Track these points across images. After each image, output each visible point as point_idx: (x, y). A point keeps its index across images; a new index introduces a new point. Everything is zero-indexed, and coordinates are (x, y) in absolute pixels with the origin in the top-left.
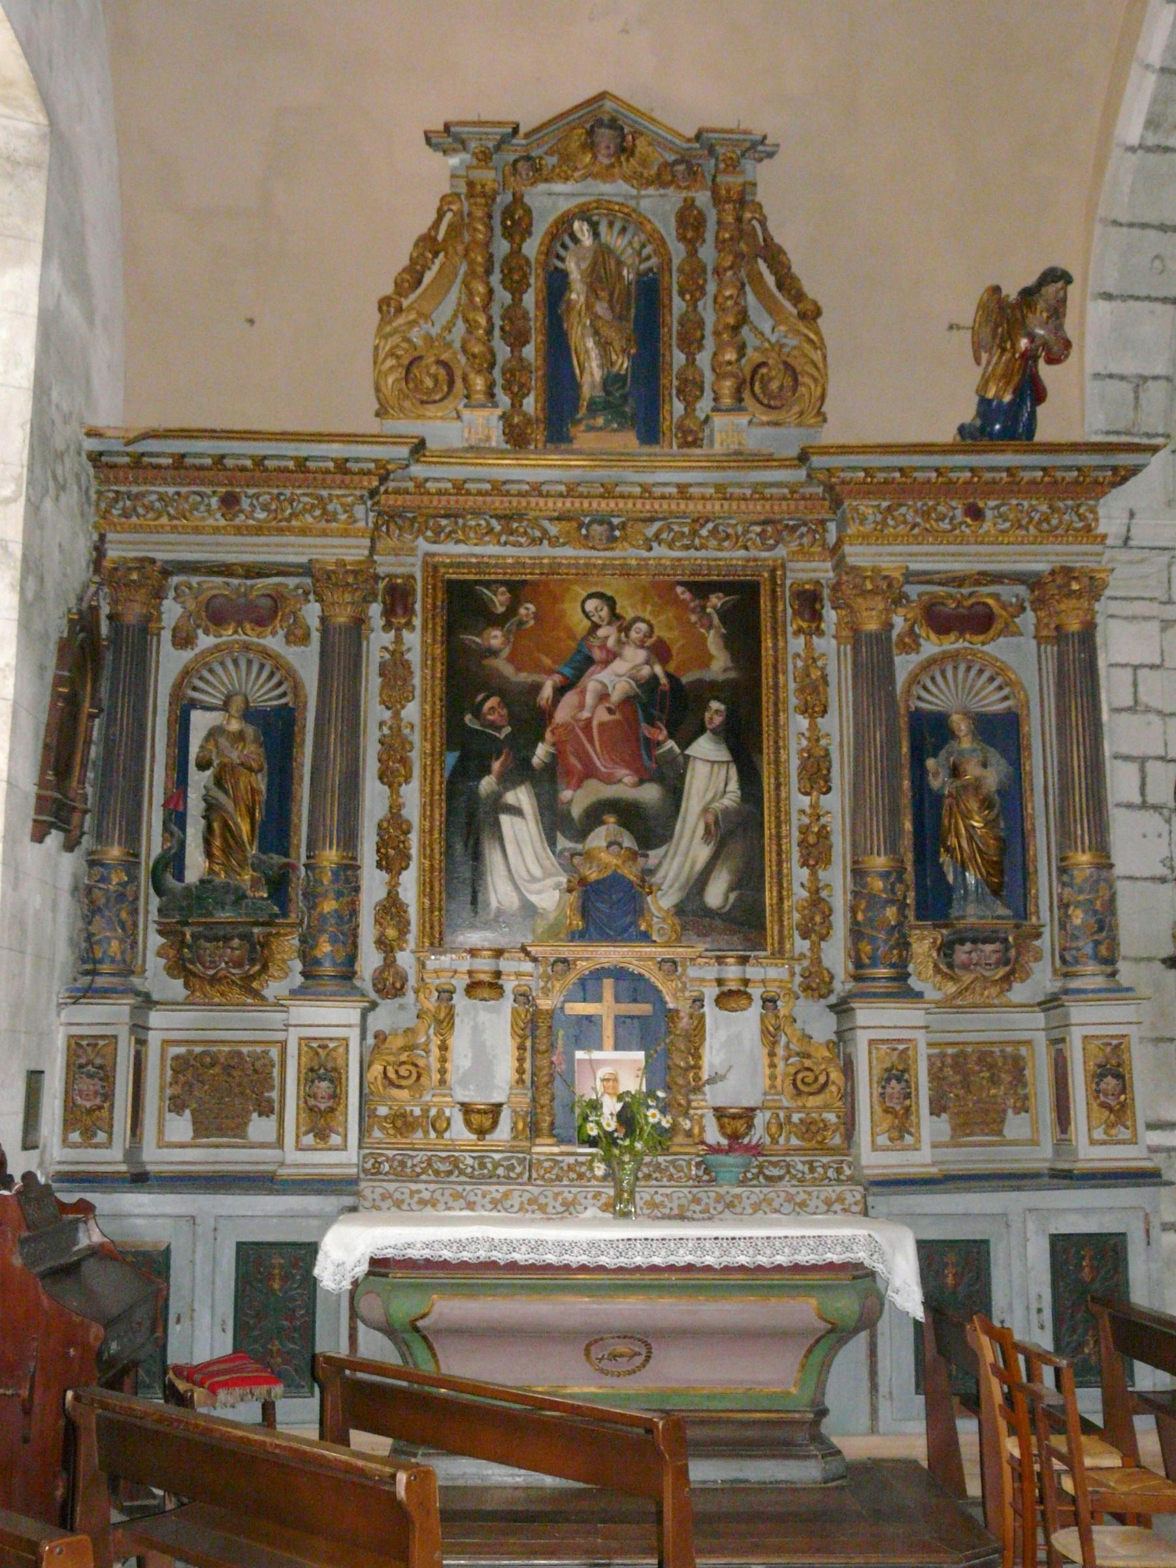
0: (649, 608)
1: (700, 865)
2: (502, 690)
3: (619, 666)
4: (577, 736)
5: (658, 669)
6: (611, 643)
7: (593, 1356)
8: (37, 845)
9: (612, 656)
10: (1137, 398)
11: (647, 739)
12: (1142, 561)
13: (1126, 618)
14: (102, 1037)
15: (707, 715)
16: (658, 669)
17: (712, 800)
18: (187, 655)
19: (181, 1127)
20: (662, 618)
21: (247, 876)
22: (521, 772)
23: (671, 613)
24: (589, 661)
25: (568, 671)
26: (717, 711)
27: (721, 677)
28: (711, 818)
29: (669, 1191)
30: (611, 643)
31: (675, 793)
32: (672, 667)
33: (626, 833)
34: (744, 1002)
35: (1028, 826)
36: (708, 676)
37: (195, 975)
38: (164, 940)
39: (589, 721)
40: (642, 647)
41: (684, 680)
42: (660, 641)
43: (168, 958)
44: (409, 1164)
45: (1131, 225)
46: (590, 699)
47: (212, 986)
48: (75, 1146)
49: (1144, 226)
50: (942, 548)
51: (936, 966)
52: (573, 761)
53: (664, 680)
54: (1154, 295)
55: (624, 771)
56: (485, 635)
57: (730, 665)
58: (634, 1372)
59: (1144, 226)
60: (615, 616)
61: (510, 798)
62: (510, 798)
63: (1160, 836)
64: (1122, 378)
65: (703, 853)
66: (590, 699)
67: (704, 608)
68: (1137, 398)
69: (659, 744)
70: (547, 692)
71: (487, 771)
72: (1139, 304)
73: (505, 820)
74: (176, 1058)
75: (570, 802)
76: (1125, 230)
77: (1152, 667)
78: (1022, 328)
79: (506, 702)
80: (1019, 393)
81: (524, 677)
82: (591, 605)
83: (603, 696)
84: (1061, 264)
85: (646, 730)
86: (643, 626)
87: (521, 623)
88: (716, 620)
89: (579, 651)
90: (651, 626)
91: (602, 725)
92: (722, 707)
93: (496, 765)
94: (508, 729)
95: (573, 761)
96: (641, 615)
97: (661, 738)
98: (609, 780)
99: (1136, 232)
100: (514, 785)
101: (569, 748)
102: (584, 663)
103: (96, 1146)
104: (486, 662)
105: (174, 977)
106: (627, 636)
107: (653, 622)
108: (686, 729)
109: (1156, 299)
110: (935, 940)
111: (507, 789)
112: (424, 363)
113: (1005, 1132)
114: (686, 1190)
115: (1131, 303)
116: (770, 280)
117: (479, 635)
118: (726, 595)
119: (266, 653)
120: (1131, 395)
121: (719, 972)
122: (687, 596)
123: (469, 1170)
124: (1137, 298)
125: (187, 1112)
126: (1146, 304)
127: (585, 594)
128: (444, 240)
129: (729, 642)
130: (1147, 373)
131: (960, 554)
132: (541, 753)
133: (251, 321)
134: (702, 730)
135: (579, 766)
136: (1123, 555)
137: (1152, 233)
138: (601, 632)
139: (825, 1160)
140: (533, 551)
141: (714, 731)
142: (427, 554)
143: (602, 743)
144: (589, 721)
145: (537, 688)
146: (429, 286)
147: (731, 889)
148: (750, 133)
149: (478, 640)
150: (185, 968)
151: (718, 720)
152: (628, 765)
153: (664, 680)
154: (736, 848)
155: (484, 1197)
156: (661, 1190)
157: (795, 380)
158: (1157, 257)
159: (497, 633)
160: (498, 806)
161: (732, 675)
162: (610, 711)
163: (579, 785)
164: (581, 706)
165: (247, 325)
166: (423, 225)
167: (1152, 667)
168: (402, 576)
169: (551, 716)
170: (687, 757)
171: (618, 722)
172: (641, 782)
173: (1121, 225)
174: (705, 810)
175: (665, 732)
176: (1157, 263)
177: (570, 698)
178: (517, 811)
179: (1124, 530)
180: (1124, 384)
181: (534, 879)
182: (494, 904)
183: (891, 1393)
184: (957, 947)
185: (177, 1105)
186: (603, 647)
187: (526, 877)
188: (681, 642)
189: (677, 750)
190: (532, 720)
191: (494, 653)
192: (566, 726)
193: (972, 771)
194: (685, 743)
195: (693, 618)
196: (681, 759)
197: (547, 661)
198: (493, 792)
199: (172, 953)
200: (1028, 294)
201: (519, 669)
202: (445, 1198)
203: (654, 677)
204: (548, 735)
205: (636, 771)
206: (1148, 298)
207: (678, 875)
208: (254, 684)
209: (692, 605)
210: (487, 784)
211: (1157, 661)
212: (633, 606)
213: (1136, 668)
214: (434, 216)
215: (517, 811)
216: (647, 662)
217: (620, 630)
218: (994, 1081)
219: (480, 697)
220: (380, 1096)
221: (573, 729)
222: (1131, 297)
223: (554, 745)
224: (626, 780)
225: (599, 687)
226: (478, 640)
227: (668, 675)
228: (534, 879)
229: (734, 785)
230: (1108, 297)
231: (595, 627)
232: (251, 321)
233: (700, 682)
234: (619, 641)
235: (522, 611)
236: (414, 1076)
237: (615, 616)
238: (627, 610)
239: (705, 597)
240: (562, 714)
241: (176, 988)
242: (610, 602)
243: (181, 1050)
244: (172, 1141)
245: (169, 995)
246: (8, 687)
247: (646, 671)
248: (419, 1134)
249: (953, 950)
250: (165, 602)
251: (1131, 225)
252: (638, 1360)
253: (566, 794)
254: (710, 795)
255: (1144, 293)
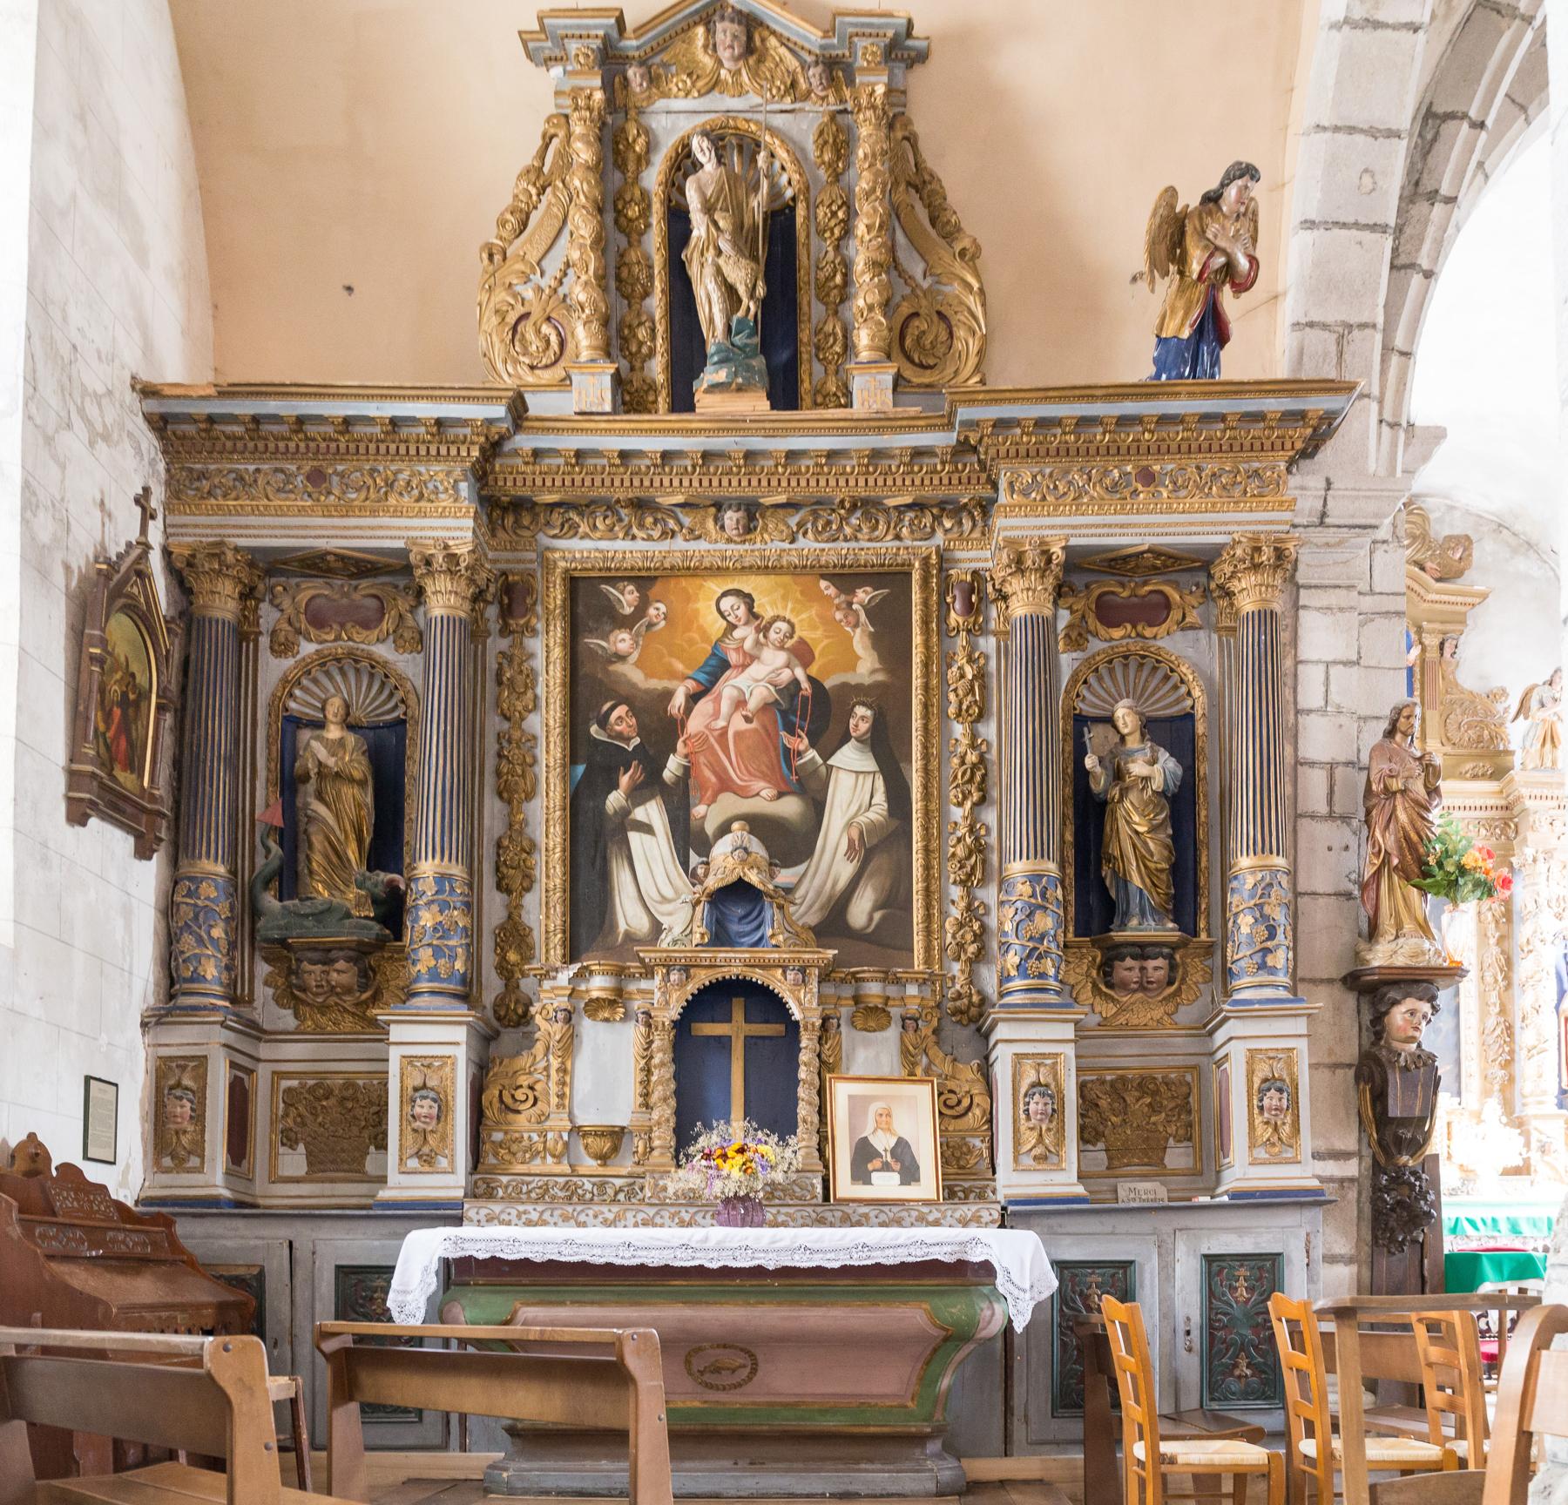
0: (790, 606)
1: (842, 883)
2: (629, 697)
3: (756, 670)
4: (712, 747)
5: (800, 673)
6: (748, 645)
7: (695, 1369)
8: (78, 829)
9: (750, 659)
10: (1341, 354)
11: (787, 750)
12: (1340, 543)
13: (1318, 609)
14: (193, 1058)
15: (852, 722)
16: (800, 673)
17: (856, 815)
18: (288, 662)
19: (294, 1161)
20: (804, 616)
21: (352, 894)
22: (650, 785)
23: (813, 611)
24: (725, 665)
25: (702, 677)
26: (863, 718)
27: (867, 681)
28: (855, 835)
29: (791, 1210)
30: (748, 645)
31: (817, 807)
32: (814, 670)
33: (755, 840)
34: (884, 1021)
35: (1201, 835)
36: (852, 679)
37: (303, 1002)
38: (270, 969)
39: (724, 731)
40: (782, 648)
41: (828, 684)
42: (802, 641)
43: (276, 987)
44: (525, 1189)
45: (1337, 129)
46: (725, 706)
47: (323, 1014)
48: (167, 1171)
49: (1352, 130)
50: (1109, 519)
51: (1095, 985)
52: (708, 773)
53: (805, 685)
54: (1363, 221)
55: (762, 784)
56: (612, 638)
57: (877, 666)
58: (740, 1385)
59: (1352, 130)
60: (753, 615)
61: (639, 814)
62: (639, 814)
63: (1347, 848)
64: (1325, 326)
65: (845, 871)
66: (725, 706)
67: (850, 604)
68: (1341, 354)
69: (800, 754)
70: (679, 700)
71: (616, 787)
72: (1344, 232)
73: (635, 838)
74: (289, 1090)
75: (704, 817)
76: (1328, 135)
77: (1346, 663)
78: (1201, 247)
79: (634, 710)
80: (1199, 332)
81: (657, 684)
82: (726, 604)
83: (740, 703)
84: (1246, 158)
85: (786, 739)
86: (784, 626)
87: (650, 625)
88: (863, 617)
89: (713, 654)
90: (792, 626)
91: (738, 734)
92: (869, 713)
93: (624, 780)
94: (637, 741)
95: (708, 773)
96: (782, 613)
97: (802, 747)
98: (742, 793)
99: (1341, 137)
100: (641, 802)
101: (702, 759)
102: (718, 667)
103: (189, 1171)
104: (612, 668)
105: (283, 1006)
106: (765, 637)
107: (794, 620)
108: (829, 736)
109: (1367, 227)
110: (1094, 959)
111: (637, 804)
112: (532, 319)
113: (1166, 1161)
114: (810, 1209)
115: (1336, 231)
116: (922, 214)
117: (605, 637)
118: (875, 589)
119: (374, 663)
120: (1333, 348)
121: (857, 989)
122: (832, 591)
123: (588, 1196)
124: (1344, 225)
125: (301, 1148)
126: (1354, 232)
127: (720, 591)
128: (551, 172)
129: (877, 641)
130: (1354, 320)
131: (1129, 525)
132: (673, 767)
133: (349, 289)
134: (845, 738)
135: (713, 779)
136: (1319, 536)
137: (1359, 138)
138: (737, 634)
139: (966, 1185)
140: (665, 545)
141: (858, 740)
142: (567, 570)
143: (739, 754)
144: (724, 731)
145: (668, 695)
146: (535, 229)
147: (876, 908)
148: (891, 15)
149: (603, 643)
150: (295, 997)
151: (864, 727)
152: (764, 777)
153: (805, 685)
154: (880, 861)
155: (596, 1217)
156: (783, 1210)
157: (951, 335)
158: (1366, 171)
159: (624, 635)
160: (624, 824)
161: (880, 677)
162: (748, 720)
163: (713, 800)
164: (716, 714)
165: (346, 293)
166: (528, 158)
167: (1346, 663)
168: (521, 573)
169: (683, 726)
170: (830, 768)
171: (756, 730)
172: (780, 795)
173: (1325, 129)
174: (849, 825)
175: (806, 741)
176: (1367, 179)
177: (704, 706)
178: (647, 829)
179: (1319, 505)
180: (1326, 334)
181: (665, 900)
182: (622, 927)
183: (1026, 1416)
184: (1117, 963)
185: (289, 1140)
186: (740, 649)
187: (658, 898)
188: (826, 642)
189: (820, 761)
190: (661, 730)
191: (621, 658)
192: (702, 738)
193: (1138, 768)
194: (826, 756)
195: (839, 616)
196: (823, 769)
197: (679, 666)
198: (622, 808)
199: (280, 981)
200: (1212, 199)
201: (648, 675)
202: (555, 1219)
203: (795, 682)
204: (680, 745)
205: (776, 785)
206: (1356, 225)
207: (819, 894)
208: (366, 697)
209: (837, 601)
210: (615, 800)
211: (1355, 658)
212: (773, 604)
213: (1328, 664)
214: (539, 142)
215: (647, 829)
216: (788, 666)
217: (758, 630)
218: (1154, 1108)
219: (606, 707)
220: (498, 1123)
221: (707, 739)
222: (1336, 223)
223: (686, 756)
224: (763, 793)
225: (735, 693)
226: (603, 643)
227: (810, 679)
228: (665, 900)
229: (880, 797)
230: (1309, 224)
231: (732, 627)
232: (349, 289)
233: (845, 685)
234: (757, 643)
235: (652, 611)
236: (531, 1101)
237: (753, 615)
238: (766, 608)
239: (852, 592)
240: (695, 724)
241: (286, 1019)
242: (748, 599)
243: (294, 1083)
244: (287, 1172)
245: (280, 1026)
246: (10, 630)
247: (786, 675)
248: (538, 1161)
249: (1112, 967)
250: (262, 605)
251: (1337, 129)
252: (745, 1372)
253: (699, 810)
254: (854, 808)
255: (1351, 220)
